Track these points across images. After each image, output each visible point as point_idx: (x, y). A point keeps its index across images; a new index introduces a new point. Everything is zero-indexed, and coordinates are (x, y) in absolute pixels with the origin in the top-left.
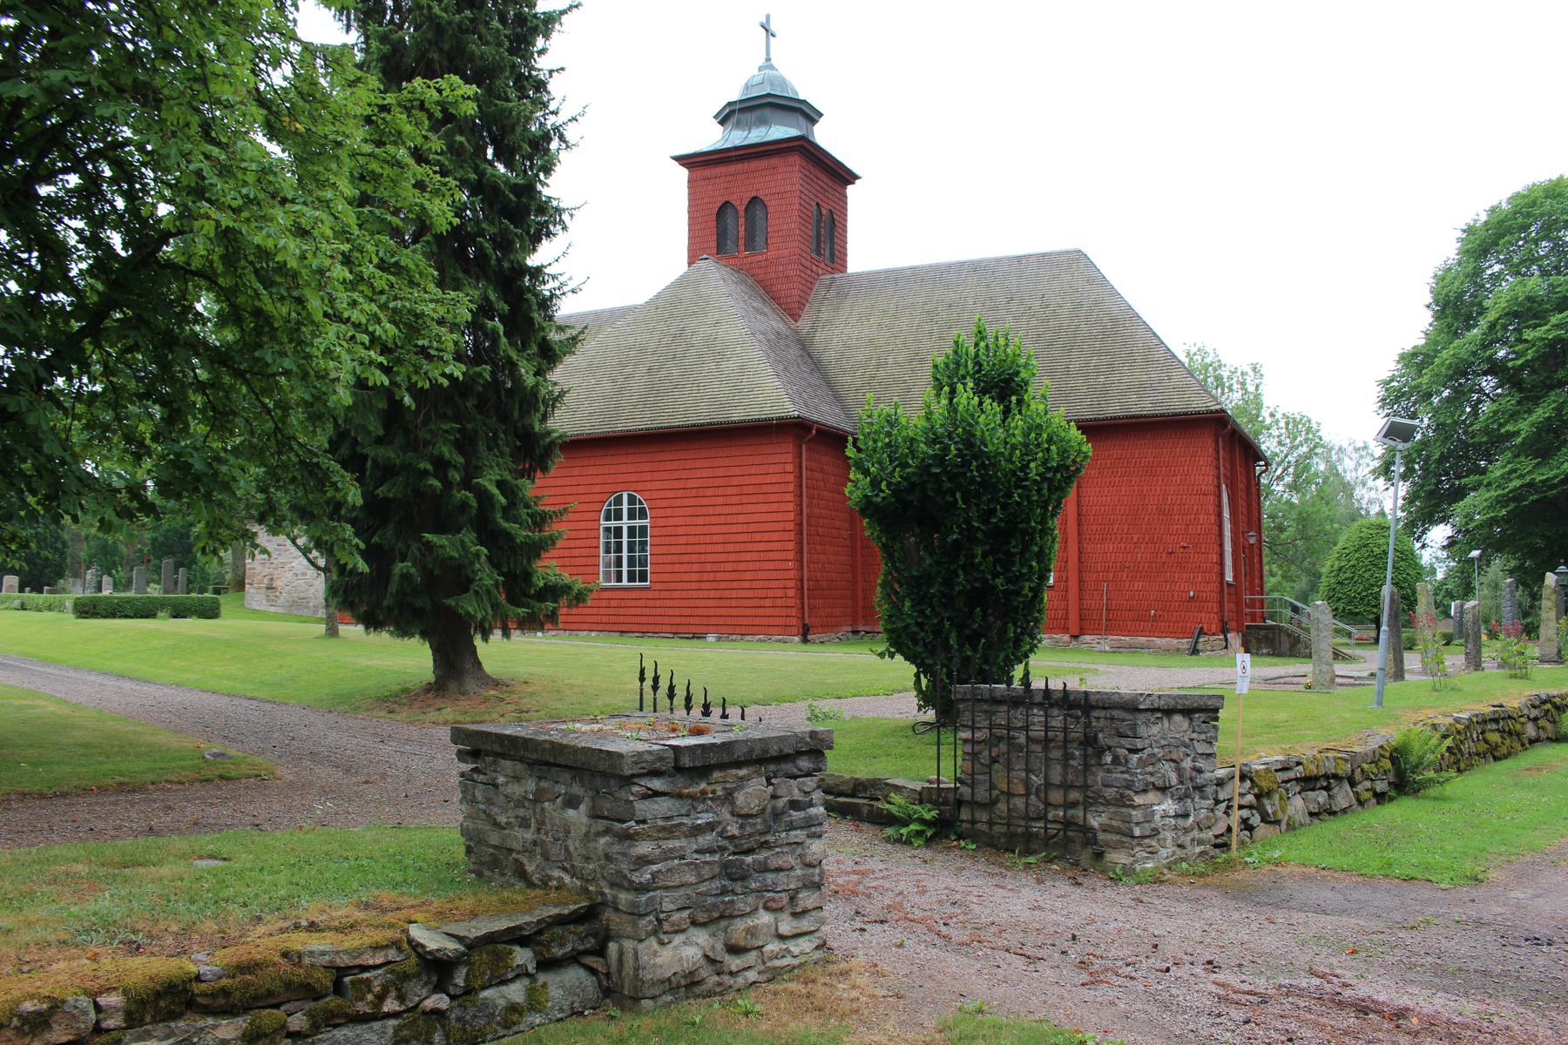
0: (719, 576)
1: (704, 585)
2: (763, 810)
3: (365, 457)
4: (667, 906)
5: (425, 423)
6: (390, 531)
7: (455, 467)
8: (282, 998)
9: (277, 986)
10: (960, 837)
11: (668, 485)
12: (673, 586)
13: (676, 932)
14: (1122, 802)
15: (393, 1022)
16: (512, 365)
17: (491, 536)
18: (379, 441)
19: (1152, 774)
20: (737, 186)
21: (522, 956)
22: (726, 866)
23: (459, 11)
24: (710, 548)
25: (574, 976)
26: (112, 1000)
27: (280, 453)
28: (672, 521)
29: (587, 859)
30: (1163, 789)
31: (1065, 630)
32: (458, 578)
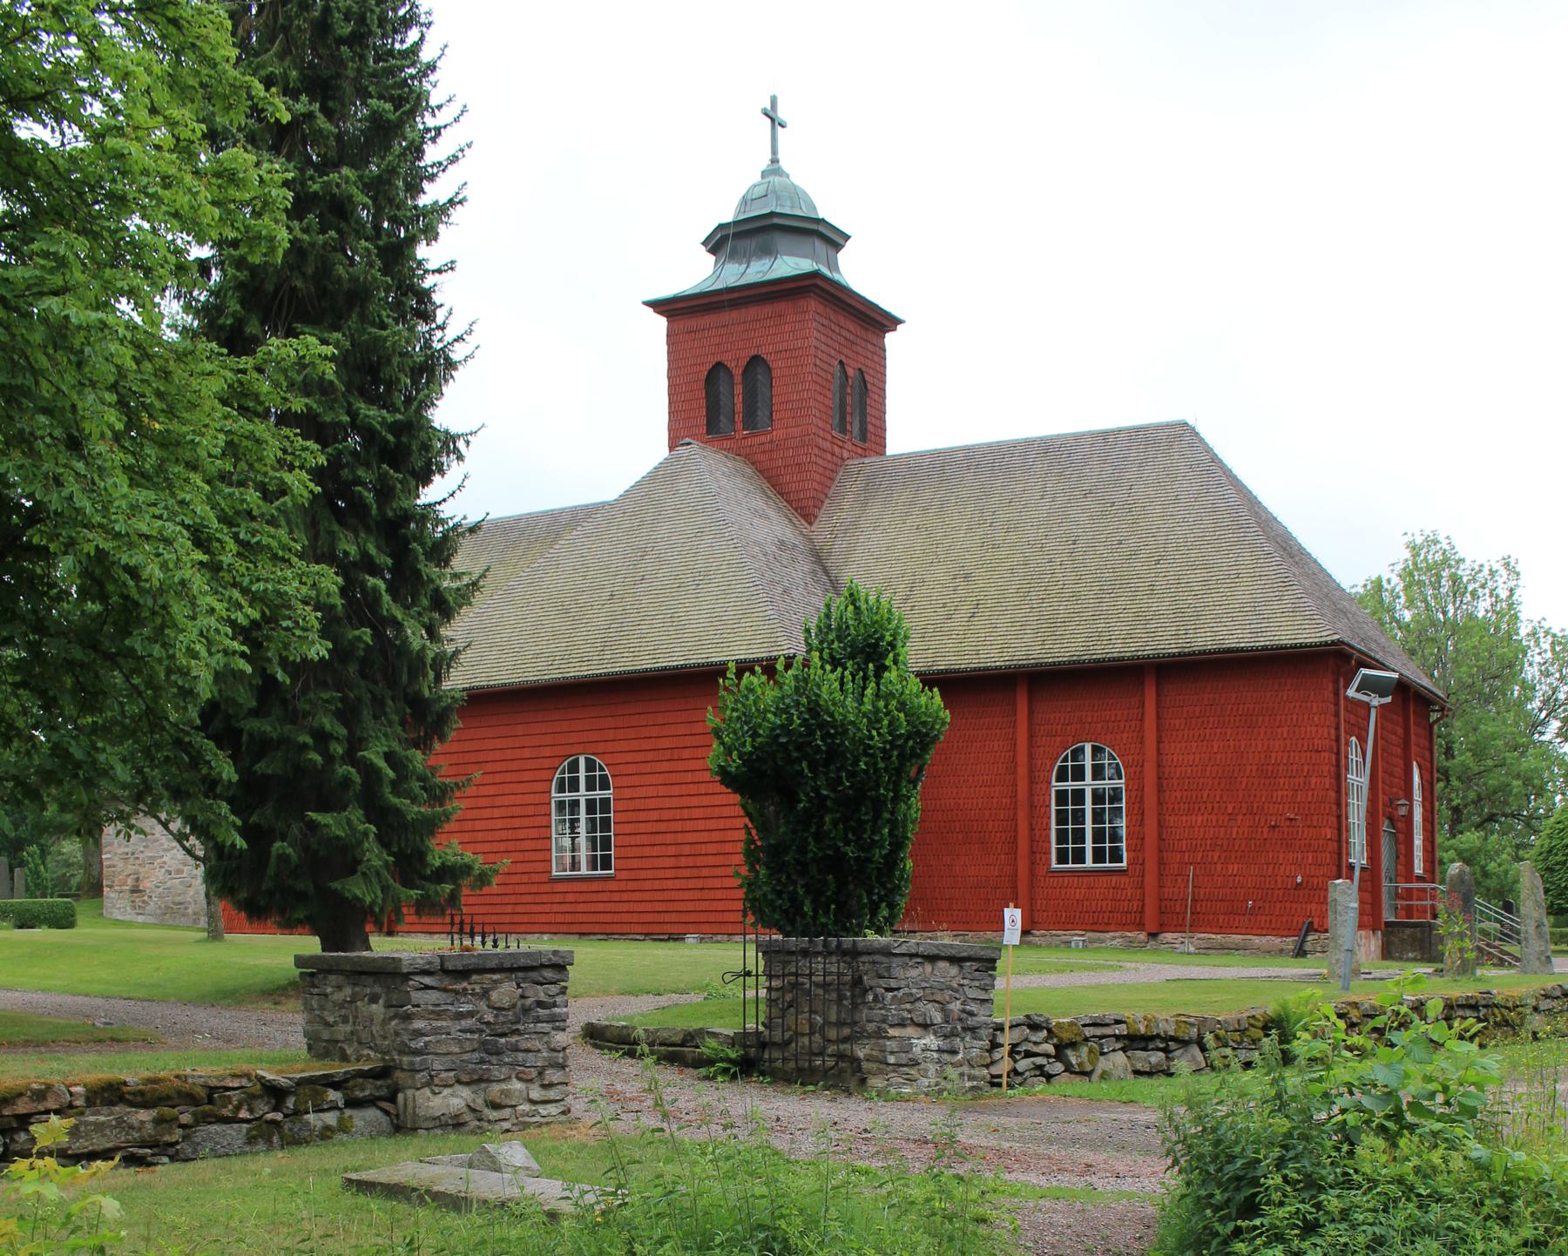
0: (700, 861)
1: (682, 873)
2: (514, 1006)
3: (241, 732)
4: (437, 1066)
5: (304, 692)
6: (269, 810)
7: (337, 739)
8: (176, 1102)
9: (172, 1093)
10: (763, 1074)
11: (634, 745)
12: (643, 874)
13: (445, 1086)
14: (879, 1034)
15: (245, 1125)
16: (398, 626)
17: (378, 812)
18: (255, 713)
19: (909, 1011)
20: (733, 341)
21: (334, 1095)
22: (484, 1043)
23: (323, 231)
24: (689, 825)
25: (372, 1113)
26: (78, 1089)
27: (152, 732)
28: (641, 792)
29: (385, 1038)
30: (925, 1026)
31: (1140, 926)
32: (346, 859)
